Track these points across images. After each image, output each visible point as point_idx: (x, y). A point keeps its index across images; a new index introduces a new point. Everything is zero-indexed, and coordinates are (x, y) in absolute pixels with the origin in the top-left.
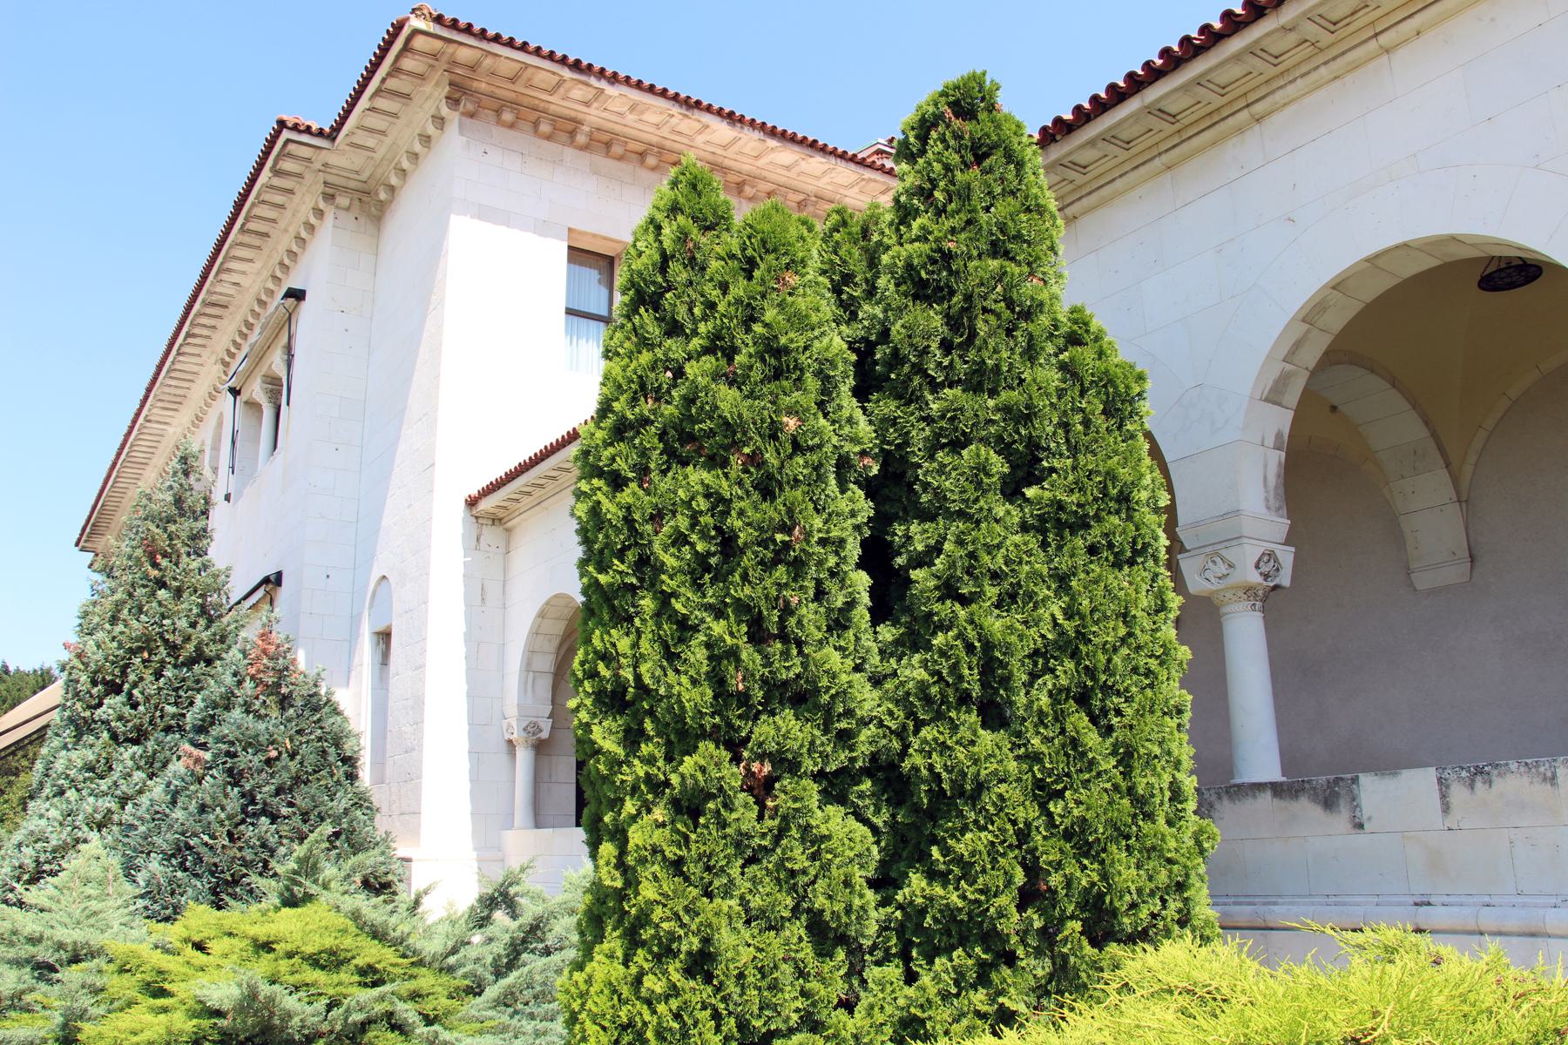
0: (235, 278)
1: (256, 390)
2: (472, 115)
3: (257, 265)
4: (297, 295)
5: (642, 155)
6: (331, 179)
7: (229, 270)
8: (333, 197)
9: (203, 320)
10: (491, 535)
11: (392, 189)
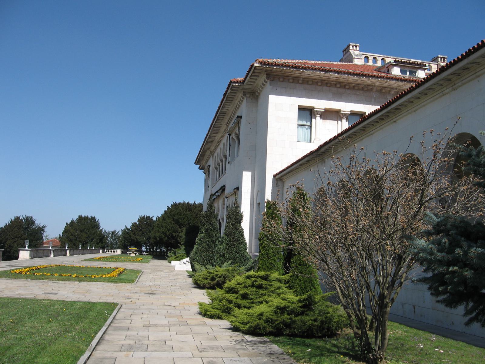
0: (226, 108)
1: (233, 135)
2: (273, 80)
3: (232, 106)
4: (240, 117)
5: (317, 83)
6: (244, 91)
7: (225, 107)
8: (245, 94)
9: (220, 116)
10: (280, 183)
11: (259, 93)
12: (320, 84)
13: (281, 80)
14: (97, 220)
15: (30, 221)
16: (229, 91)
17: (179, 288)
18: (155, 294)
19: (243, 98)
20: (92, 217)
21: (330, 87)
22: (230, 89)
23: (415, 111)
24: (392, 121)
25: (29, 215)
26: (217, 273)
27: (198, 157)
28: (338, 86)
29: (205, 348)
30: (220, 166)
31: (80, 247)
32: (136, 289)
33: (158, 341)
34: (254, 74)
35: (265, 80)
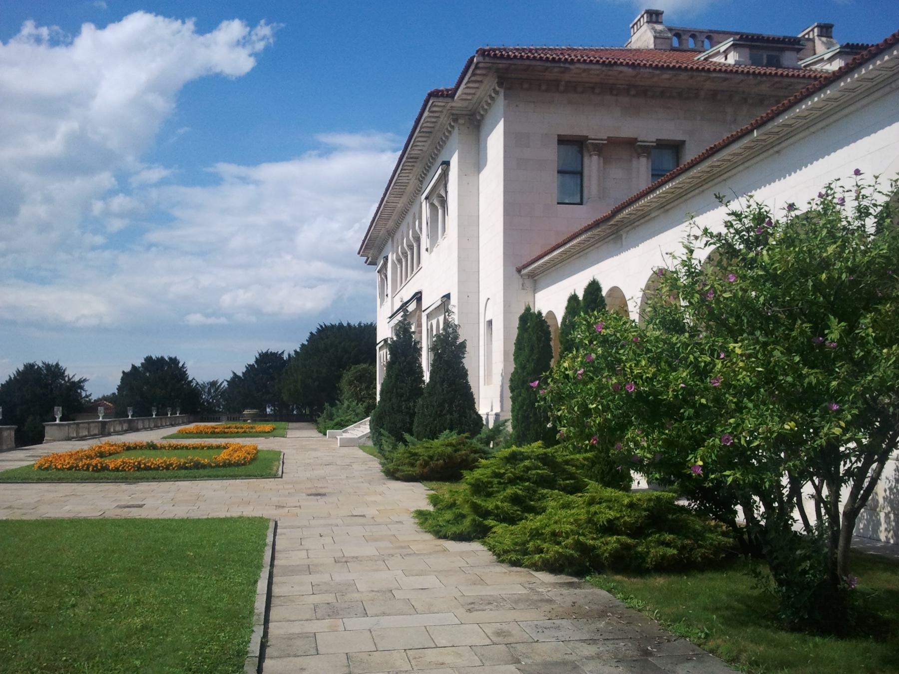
6: (454, 112)
11: (482, 116)
12: (597, 91)
13: (526, 86)
14: (180, 365)
15: (55, 372)
16: (426, 114)
17: (361, 480)
18: (324, 495)
19: (452, 127)
20: (170, 359)
21: (616, 95)
22: (427, 109)
23: (822, 128)
24: (771, 151)
25: (52, 362)
26: (431, 453)
27: (364, 241)
28: (633, 92)
29: (473, 603)
30: (406, 257)
31: (154, 414)
32: (286, 486)
33: (378, 591)
34: (473, 78)
35: (494, 89)
